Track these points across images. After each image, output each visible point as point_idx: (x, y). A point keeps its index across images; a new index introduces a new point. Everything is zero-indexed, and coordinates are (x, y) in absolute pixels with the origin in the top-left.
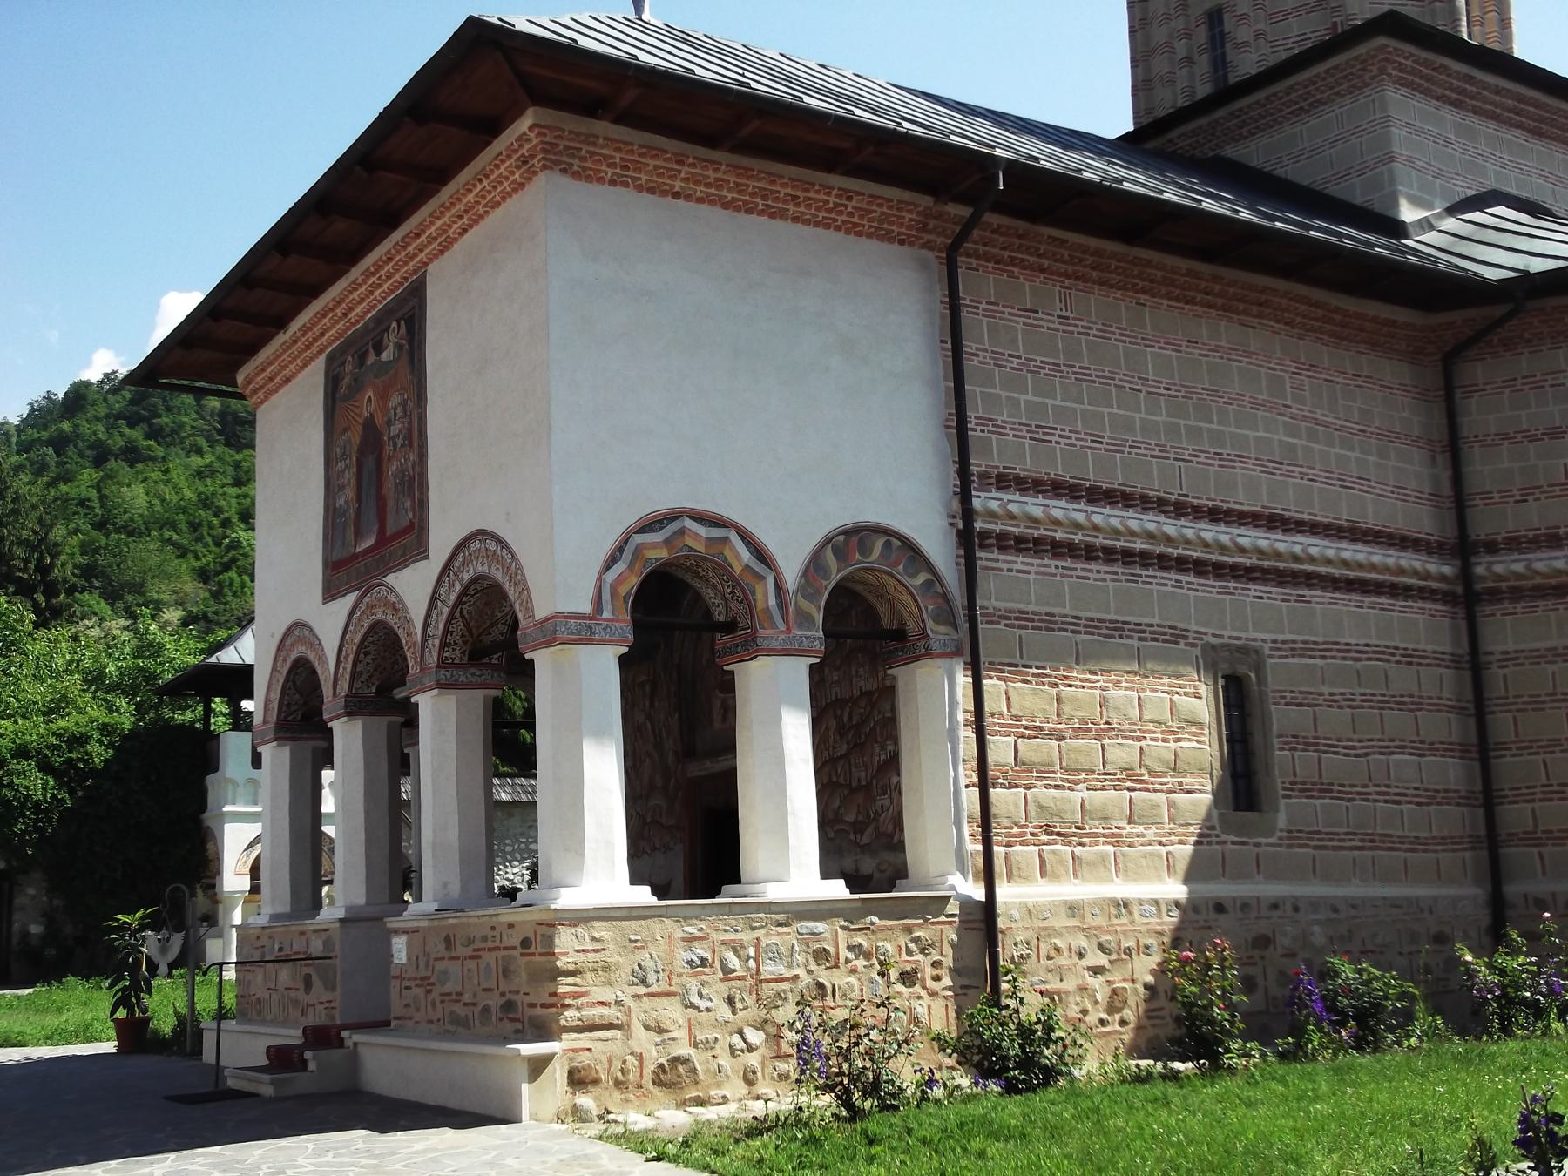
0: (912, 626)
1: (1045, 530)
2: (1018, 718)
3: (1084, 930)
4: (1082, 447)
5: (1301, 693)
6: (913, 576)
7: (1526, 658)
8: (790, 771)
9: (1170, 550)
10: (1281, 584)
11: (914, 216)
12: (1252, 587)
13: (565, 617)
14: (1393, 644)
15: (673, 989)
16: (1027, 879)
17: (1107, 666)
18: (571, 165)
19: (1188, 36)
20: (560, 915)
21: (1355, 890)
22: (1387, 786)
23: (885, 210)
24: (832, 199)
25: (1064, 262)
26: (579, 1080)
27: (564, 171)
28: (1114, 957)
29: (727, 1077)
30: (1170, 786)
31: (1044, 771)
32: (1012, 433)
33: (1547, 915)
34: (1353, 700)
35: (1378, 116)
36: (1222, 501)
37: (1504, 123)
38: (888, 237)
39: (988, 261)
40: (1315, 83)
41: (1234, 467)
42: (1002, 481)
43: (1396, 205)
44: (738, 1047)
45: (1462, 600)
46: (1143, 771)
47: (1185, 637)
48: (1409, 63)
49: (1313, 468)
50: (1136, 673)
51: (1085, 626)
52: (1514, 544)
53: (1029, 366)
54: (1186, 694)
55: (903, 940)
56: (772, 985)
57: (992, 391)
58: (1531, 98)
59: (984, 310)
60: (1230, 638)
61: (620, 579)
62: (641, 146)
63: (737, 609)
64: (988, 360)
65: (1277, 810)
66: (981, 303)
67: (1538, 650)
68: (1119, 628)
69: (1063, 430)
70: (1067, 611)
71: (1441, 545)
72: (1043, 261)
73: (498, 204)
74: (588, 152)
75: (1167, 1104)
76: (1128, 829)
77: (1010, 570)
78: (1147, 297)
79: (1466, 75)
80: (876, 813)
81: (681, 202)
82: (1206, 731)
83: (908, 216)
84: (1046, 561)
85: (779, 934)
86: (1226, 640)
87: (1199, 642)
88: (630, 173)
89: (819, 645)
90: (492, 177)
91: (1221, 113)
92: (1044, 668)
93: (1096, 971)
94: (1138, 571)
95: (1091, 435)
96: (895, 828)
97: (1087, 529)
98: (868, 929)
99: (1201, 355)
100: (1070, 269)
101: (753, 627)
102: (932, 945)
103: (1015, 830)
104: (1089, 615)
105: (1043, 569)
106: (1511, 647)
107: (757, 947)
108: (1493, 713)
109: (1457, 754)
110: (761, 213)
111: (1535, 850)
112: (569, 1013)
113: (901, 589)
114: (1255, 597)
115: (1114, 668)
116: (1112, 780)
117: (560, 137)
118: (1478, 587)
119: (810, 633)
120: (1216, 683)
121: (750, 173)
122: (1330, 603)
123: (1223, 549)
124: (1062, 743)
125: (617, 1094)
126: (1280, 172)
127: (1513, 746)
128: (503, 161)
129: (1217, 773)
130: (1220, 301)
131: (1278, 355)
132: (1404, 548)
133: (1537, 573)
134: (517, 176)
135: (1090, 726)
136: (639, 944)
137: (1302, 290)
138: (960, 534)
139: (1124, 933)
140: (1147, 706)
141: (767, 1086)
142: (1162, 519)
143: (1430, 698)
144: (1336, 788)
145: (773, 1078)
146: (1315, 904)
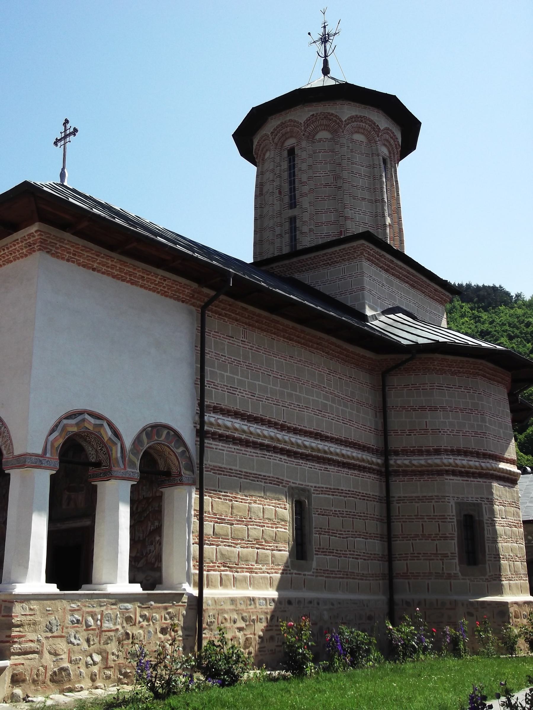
0: (174, 470)
1: (231, 432)
2: (215, 514)
3: (236, 611)
4: (247, 397)
5: (324, 510)
6: (177, 448)
7: (407, 500)
8: (120, 532)
9: (278, 445)
10: (319, 463)
11: (189, 291)
12: (308, 463)
13: (31, 455)
14: (358, 491)
15: (63, 634)
16: (215, 587)
17: (252, 493)
18: (51, 250)
19: (281, 226)
20: (17, 597)
21: (340, 596)
22: (354, 551)
23: (178, 287)
24: (158, 280)
25: (246, 318)
26: (16, 680)
27: (48, 252)
28: (248, 623)
29: (84, 677)
30: (273, 548)
31: (225, 537)
32: (221, 389)
33: (418, 609)
34: (343, 514)
35: (359, 271)
36: (299, 425)
37: (402, 280)
38: (178, 299)
39: (216, 314)
40: (335, 254)
41: (304, 411)
42: (216, 410)
43: (364, 308)
44: (90, 663)
45: (385, 474)
46: (263, 540)
47: (282, 483)
48: (372, 252)
49: (333, 414)
50: (262, 497)
51: (244, 475)
52: (405, 452)
53: (229, 360)
54: (281, 508)
55: (163, 613)
56: (107, 633)
57: (214, 370)
58: (412, 272)
59: (213, 334)
60: (299, 484)
61: (55, 439)
62: (83, 246)
63: (102, 457)
64: (213, 356)
65: (313, 560)
66: (212, 331)
67: (412, 497)
68: (257, 477)
69: (240, 389)
70: (238, 468)
71: (377, 450)
72: (237, 316)
73: (11, 261)
74: (60, 245)
75: (289, 691)
76: (256, 566)
77: (216, 449)
78: (275, 336)
79: (391, 260)
80: (147, 553)
81: (95, 273)
82: (288, 524)
83: (187, 291)
84: (231, 446)
85: (112, 609)
86: (297, 485)
87: (287, 486)
88: (76, 257)
89: (137, 476)
90: (10, 249)
91: (295, 260)
92: (227, 493)
93: (240, 629)
94: (266, 453)
95: (251, 393)
96: (156, 561)
97: (248, 433)
98: (149, 607)
99: (294, 363)
100: (247, 321)
101: (110, 466)
102: (175, 616)
103: (211, 564)
104: (245, 470)
105: (229, 449)
106: (402, 495)
107: (102, 615)
108: (394, 522)
109: (379, 539)
110: (128, 282)
111: (407, 581)
112: (15, 646)
113: (171, 453)
114: (309, 467)
115: (254, 494)
116: (251, 544)
117: (49, 237)
118: (391, 469)
119: (133, 470)
120: (292, 503)
121: (126, 264)
122: (336, 472)
123: (298, 446)
124: (232, 527)
125: (33, 687)
126: (317, 288)
127: (400, 536)
128: (18, 243)
129: (291, 543)
130: (303, 341)
131: (323, 366)
132: (364, 451)
133: (414, 465)
134: (24, 251)
135: (244, 519)
136: (50, 612)
137: (334, 340)
138: (197, 431)
139: (252, 612)
140: (266, 512)
141: (101, 682)
142: (276, 431)
143: (371, 515)
144: (335, 551)
145: (103, 678)
146: (325, 601)
